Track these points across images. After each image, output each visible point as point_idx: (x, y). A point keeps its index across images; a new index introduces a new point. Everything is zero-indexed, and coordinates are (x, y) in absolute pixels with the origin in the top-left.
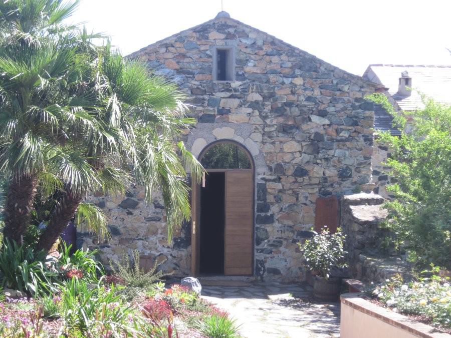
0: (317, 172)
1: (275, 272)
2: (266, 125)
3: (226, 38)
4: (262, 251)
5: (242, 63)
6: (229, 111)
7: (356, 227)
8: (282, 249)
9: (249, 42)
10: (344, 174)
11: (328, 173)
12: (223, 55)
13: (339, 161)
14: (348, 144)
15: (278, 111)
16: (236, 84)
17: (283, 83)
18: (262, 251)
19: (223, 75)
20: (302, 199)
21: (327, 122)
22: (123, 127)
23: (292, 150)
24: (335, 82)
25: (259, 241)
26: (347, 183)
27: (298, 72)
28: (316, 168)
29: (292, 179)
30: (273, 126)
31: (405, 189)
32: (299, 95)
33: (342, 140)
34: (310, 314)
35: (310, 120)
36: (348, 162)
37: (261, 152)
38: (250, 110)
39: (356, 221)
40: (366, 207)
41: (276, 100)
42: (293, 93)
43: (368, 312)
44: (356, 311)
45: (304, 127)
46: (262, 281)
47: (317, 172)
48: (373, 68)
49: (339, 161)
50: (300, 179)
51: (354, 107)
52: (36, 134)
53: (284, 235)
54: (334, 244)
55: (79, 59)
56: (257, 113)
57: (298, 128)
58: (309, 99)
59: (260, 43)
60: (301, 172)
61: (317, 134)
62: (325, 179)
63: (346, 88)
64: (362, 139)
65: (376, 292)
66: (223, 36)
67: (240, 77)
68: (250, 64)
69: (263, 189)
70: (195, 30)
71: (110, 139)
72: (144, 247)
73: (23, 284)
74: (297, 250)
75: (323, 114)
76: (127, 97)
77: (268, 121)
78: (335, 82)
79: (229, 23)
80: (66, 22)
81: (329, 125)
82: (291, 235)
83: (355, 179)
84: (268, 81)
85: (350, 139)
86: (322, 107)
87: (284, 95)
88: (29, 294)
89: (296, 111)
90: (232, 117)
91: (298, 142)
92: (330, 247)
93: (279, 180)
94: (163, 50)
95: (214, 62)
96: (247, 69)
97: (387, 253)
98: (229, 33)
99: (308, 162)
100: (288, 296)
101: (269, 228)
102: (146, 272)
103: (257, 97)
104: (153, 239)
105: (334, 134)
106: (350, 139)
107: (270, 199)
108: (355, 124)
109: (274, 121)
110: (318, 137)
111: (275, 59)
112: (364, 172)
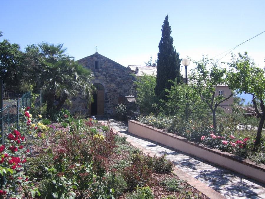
0: (119, 91)
1: (109, 114)
2: (107, 80)
3: (98, 59)
4: (106, 109)
5: (101, 65)
6: (98, 76)
7: (128, 104)
8: (111, 109)
9: (103, 60)
10: (125, 91)
11: (121, 91)
12: (97, 63)
13: (124, 88)
14: (126, 84)
15: (110, 76)
16: (100, 70)
17: (111, 70)
18: (106, 109)
19: (96, 67)
20: (115, 97)
21: (121, 79)
22: (79, 80)
23: (113, 85)
24: (123, 70)
25: (105, 107)
26: (126, 93)
27: (114, 67)
28: (119, 90)
29: (113, 92)
30: (108, 80)
31: (141, 95)
32: (115, 73)
33: (125, 83)
34: (119, 124)
35: (117, 78)
36: (126, 88)
37: (106, 86)
38: (103, 76)
39: (129, 102)
40: (130, 99)
41: (109, 74)
42: (113, 72)
43: (136, 123)
44: (133, 123)
45: (116, 80)
46: (106, 116)
47: (119, 91)
48: (129, 66)
49: (124, 88)
50: (115, 92)
51: (127, 76)
52: (58, 82)
53: (112, 105)
54: (123, 108)
55: (68, 63)
56: (105, 77)
57: (114, 80)
58: (117, 74)
59: (105, 60)
60: (115, 91)
61: (119, 82)
62: (121, 92)
63: (126, 71)
64: (129, 83)
65: (137, 119)
66: (97, 58)
67: (101, 68)
68: (103, 65)
69: (106, 94)
70: (90, 56)
71: (76, 83)
72: (78, 109)
73: (55, 119)
74: (115, 109)
75: (120, 77)
76: (79, 73)
77: (107, 79)
78: (123, 70)
79: (98, 55)
80: (63, 54)
81: (122, 80)
82: (113, 105)
83: (128, 92)
84: (107, 69)
85: (126, 83)
86: (120, 75)
87: (111, 73)
88: (57, 122)
89: (114, 76)
90: (99, 78)
91: (115, 84)
92: (123, 108)
93: (110, 93)
94: (82, 61)
95: (94, 65)
96: (102, 66)
97: (136, 110)
98: (98, 57)
99: (117, 88)
100: (112, 120)
101: (108, 104)
102: (83, 115)
103: (105, 73)
104: (80, 107)
105: (123, 82)
106: (126, 83)
107: (108, 97)
108: (128, 79)
109: (109, 79)
110: (119, 82)
111: (109, 64)
112: (129, 91)
